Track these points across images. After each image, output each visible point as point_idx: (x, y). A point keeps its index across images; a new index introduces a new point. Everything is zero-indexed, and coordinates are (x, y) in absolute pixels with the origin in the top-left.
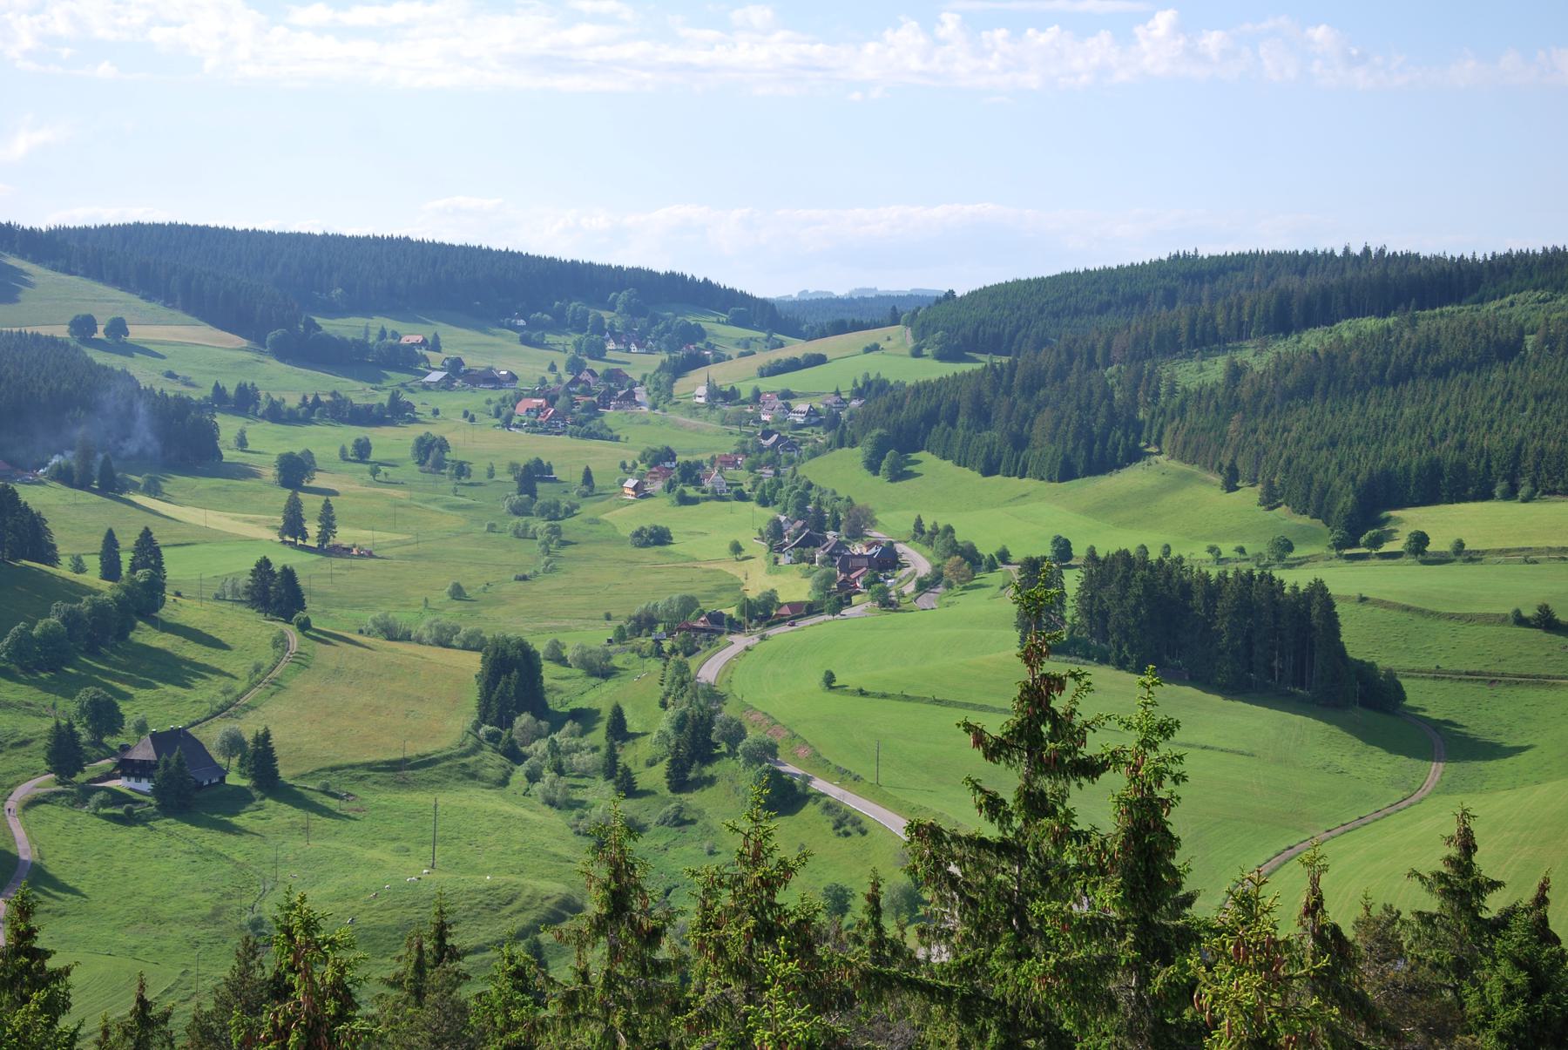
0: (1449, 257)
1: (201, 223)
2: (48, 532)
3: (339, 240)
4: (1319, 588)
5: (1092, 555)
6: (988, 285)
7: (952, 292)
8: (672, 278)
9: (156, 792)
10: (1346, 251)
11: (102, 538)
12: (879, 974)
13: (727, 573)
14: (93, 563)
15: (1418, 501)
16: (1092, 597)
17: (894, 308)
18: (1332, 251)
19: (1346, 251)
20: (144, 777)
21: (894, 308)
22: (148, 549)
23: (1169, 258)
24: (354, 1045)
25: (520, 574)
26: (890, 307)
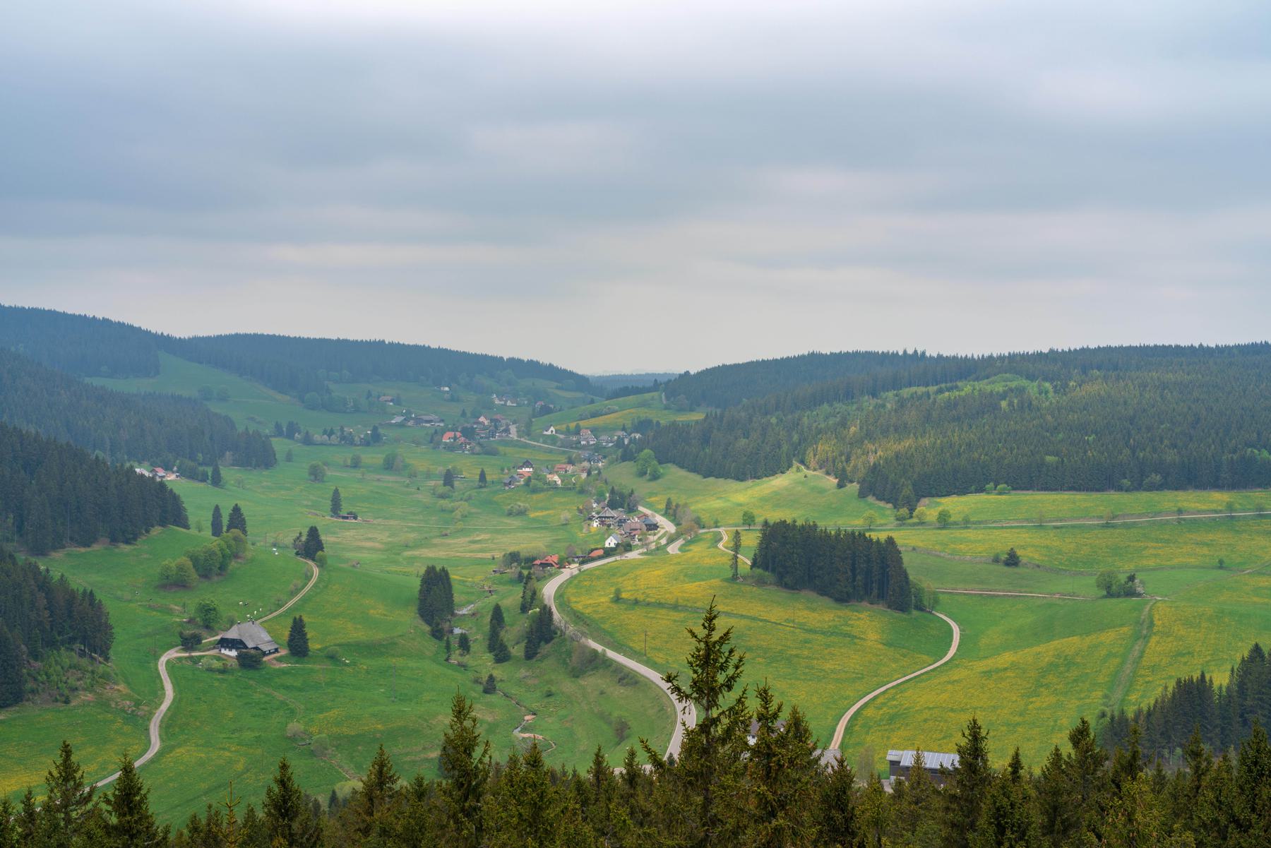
0: (960, 357)
1: (271, 333)
2: (185, 510)
3: (346, 341)
4: (890, 541)
5: (766, 523)
6: (708, 368)
7: (688, 372)
8: (531, 363)
9: (238, 657)
10: (905, 352)
11: (212, 513)
12: (213, 478)
13: (697, 715)
14: (207, 524)
15: (846, 740)
16: (766, 548)
17: (656, 380)
18: (897, 353)
19: (905, 352)
20: (234, 648)
21: (656, 380)
22: (237, 519)
23: (808, 354)
24: (700, 847)
25: (443, 533)
26: (654, 379)
